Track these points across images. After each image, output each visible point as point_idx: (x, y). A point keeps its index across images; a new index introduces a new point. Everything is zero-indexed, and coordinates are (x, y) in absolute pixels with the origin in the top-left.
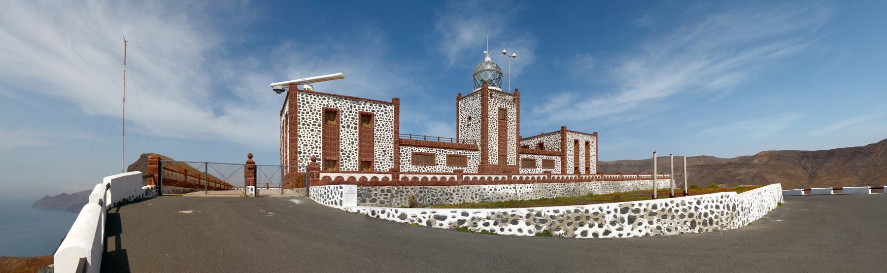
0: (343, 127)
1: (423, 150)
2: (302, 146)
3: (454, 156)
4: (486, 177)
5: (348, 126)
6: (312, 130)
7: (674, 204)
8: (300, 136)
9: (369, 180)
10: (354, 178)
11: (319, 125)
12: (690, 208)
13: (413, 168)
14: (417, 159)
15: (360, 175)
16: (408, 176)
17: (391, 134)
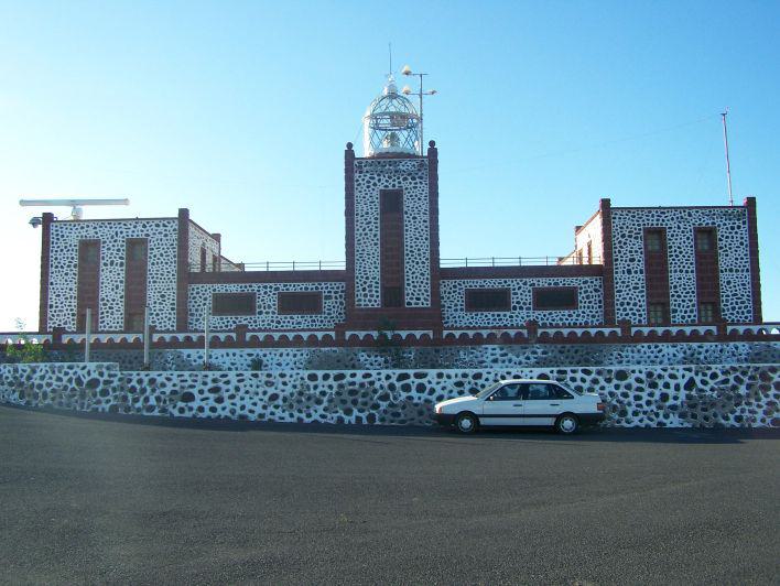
0: (105, 265)
1: (234, 288)
3: (294, 295)
4: (389, 334)
5: (112, 263)
6: (66, 274)
8: (52, 284)
9: (167, 340)
11: (75, 266)
12: (22, 376)
13: (216, 320)
14: (223, 305)
15: (663, 329)
16: (302, 334)
17: (173, 268)
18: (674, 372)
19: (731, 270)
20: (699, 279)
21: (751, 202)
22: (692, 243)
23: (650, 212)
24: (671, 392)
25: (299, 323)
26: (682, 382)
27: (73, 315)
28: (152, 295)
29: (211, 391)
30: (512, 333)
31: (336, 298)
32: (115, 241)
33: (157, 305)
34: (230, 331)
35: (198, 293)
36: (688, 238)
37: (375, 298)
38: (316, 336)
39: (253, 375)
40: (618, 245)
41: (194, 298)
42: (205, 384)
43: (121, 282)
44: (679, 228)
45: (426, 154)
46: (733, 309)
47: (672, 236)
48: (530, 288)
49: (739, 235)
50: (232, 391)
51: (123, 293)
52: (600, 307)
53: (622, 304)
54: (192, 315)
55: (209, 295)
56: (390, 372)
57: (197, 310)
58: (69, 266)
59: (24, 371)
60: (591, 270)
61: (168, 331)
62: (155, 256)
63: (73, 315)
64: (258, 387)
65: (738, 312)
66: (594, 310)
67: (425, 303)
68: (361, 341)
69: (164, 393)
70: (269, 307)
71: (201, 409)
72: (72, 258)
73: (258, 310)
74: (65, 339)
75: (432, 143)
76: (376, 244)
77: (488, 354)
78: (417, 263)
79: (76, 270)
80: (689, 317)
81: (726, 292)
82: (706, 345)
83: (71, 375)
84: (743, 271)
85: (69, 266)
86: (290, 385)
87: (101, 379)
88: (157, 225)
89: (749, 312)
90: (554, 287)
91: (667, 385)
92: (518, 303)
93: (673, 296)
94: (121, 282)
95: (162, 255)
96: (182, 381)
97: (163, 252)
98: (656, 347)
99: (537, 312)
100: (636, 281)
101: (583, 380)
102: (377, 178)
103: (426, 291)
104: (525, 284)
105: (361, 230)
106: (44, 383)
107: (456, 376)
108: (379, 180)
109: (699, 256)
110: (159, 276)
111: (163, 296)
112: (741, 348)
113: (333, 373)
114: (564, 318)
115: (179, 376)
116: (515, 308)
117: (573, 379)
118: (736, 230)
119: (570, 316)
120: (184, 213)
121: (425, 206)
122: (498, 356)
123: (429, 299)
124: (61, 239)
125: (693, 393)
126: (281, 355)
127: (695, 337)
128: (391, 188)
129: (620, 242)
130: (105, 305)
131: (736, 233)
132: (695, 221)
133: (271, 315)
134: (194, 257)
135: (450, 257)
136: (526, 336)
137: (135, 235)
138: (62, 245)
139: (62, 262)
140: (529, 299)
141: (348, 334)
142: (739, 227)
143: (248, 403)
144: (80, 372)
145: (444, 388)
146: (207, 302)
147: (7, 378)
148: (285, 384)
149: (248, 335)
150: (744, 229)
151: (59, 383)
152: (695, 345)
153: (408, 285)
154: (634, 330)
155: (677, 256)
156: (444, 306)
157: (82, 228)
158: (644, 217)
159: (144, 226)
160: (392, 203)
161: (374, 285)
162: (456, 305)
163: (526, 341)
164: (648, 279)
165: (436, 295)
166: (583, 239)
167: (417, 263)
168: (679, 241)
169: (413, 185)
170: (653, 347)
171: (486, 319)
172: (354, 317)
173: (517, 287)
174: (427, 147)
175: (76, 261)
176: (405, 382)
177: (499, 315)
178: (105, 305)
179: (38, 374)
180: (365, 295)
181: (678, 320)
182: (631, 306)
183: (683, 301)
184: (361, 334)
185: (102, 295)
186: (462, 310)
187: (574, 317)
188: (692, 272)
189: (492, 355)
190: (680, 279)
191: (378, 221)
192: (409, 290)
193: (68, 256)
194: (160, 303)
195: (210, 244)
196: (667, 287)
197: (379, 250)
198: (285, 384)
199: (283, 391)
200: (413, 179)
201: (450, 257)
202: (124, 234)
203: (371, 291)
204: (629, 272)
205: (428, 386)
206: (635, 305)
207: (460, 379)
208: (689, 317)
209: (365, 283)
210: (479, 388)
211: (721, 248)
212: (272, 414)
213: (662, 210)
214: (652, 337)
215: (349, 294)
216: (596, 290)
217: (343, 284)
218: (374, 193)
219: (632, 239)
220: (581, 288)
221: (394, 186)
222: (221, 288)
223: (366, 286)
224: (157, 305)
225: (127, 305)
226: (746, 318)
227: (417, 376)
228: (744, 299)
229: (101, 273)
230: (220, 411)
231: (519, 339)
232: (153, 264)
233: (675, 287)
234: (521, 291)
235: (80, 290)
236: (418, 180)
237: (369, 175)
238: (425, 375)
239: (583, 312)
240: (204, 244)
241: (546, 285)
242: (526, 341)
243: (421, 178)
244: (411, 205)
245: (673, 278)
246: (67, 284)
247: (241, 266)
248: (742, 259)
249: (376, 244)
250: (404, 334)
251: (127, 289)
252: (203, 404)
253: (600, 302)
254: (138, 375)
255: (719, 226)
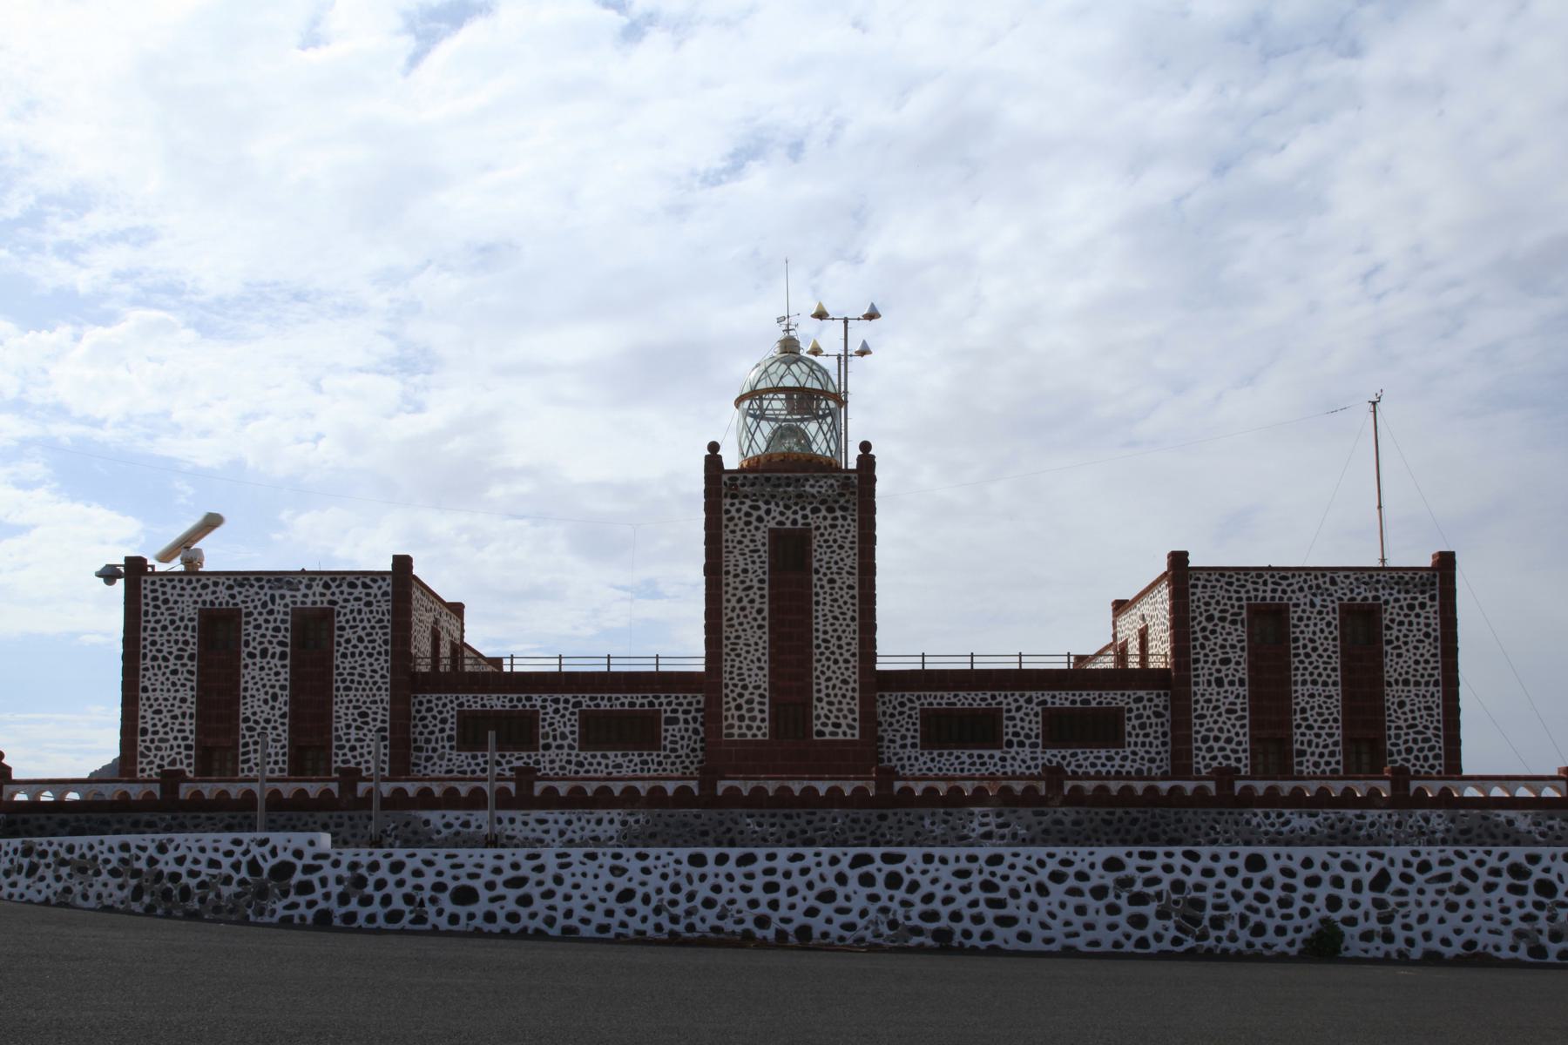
0: (251, 655)
1: (497, 702)
2: (149, 714)
5: (264, 653)
6: (174, 672)
7: (104, 848)
8: (145, 690)
10: (635, 790)
11: (191, 657)
17: (383, 663)
18: (1352, 858)
19: (1406, 682)
20: (1348, 697)
21: (1446, 562)
22: (1336, 633)
23: (1260, 576)
24: (1346, 894)
25: (619, 767)
26: (1367, 877)
27: (188, 747)
28: (343, 712)
29: (507, 884)
30: (1018, 787)
31: (686, 721)
32: (271, 612)
33: (352, 731)
34: (1031, 777)
35: (429, 710)
36: (1329, 624)
37: (758, 723)
38: (663, 790)
39: (587, 856)
40: (1199, 635)
41: (423, 718)
42: (497, 871)
43: (283, 688)
44: (1313, 605)
45: (853, 465)
46: (1409, 751)
47: (1300, 619)
48: (1039, 709)
49: (1422, 620)
50: (550, 885)
51: (286, 709)
52: (1164, 744)
53: (1205, 740)
54: (420, 749)
55: (450, 713)
56: (837, 851)
57: (428, 741)
58: (179, 658)
59: (144, 849)
60: (1147, 678)
61: (1139, 775)
62: (348, 641)
63: (188, 747)
64: (596, 876)
65: (1417, 758)
66: (1153, 750)
67: (849, 731)
68: (465, 799)
69: (419, 888)
70: (564, 737)
71: (490, 917)
72: (186, 643)
73: (542, 742)
74: (185, 791)
75: (866, 446)
76: (760, 627)
77: (975, 824)
78: (836, 662)
79: (193, 666)
80: (1328, 763)
81: (1396, 720)
82: (1372, 814)
83: (238, 855)
84: (1427, 684)
85: (179, 658)
86: (656, 874)
87: (299, 864)
88: (352, 585)
89: (1436, 757)
90: (1079, 702)
91: (1338, 882)
92: (1016, 734)
93: (1299, 726)
94: (283, 688)
95: (360, 639)
96: (454, 866)
97: (363, 634)
98: (1280, 815)
99: (1049, 752)
100: (1232, 698)
101: (1186, 870)
102: (764, 507)
103: (852, 711)
104: (1029, 701)
105: (734, 600)
106: (182, 870)
107: (957, 859)
108: (768, 512)
109: (1348, 657)
110: (356, 678)
111: (363, 715)
112: (1434, 821)
113: (735, 853)
114: (1099, 762)
115: (448, 857)
116: (1010, 744)
117: (1168, 869)
118: (1417, 610)
119: (1109, 758)
120: (403, 563)
121: (851, 560)
122: (993, 827)
123: (857, 724)
124: (163, 608)
125: (1386, 896)
126: (599, 822)
127: (1348, 799)
128: (788, 525)
129: (1204, 629)
130: (250, 729)
131: (1418, 616)
132: (1342, 592)
133: (566, 751)
134: (421, 644)
135: (896, 648)
136: (1043, 793)
137: (309, 601)
138: (166, 619)
139: (165, 649)
140: (1037, 728)
141: (722, 786)
142: (1423, 606)
143: (577, 905)
144: (256, 851)
145: (934, 881)
146: (447, 726)
147: (107, 861)
148: (646, 871)
149: (539, 787)
150: (1433, 609)
151: (214, 871)
152: (1350, 813)
153: (819, 700)
154: (1239, 785)
155: (1308, 655)
156: (882, 739)
157: (205, 587)
158: (1250, 586)
159: (327, 586)
160: (791, 556)
161: (757, 699)
162: (904, 737)
163: (1043, 801)
164: (1254, 696)
165: (869, 719)
166: (1129, 627)
167: (836, 662)
168: (1312, 628)
169: (829, 522)
170: (1273, 815)
171: (961, 765)
172: (719, 756)
173: (1013, 706)
174: (854, 453)
175: (192, 649)
176: (865, 869)
177: (980, 757)
178: (250, 729)
179: (171, 855)
180: (741, 718)
181: (1308, 768)
182: (1221, 743)
183: (1318, 736)
184: (746, 787)
185: (245, 711)
186: (914, 745)
187: (1117, 762)
188: (1335, 684)
189: (982, 825)
190: (1312, 696)
191: (766, 586)
192: (821, 709)
193: (176, 638)
194: (358, 728)
195: (447, 622)
196: (1289, 712)
197: (766, 637)
198: (646, 871)
199: (643, 884)
200: (831, 510)
201: (896, 648)
202: (288, 600)
203: (750, 710)
204: (1219, 682)
205: (907, 878)
206: (1229, 740)
207: (964, 865)
208: (1328, 763)
209: (741, 695)
210: (997, 880)
211: (1389, 642)
212: (623, 925)
213: (1282, 574)
214: (1272, 799)
215: (712, 716)
216: (1158, 715)
217: (700, 697)
218: (759, 535)
219: (1227, 625)
220: (1130, 710)
221: (795, 522)
222: (474, 702)
223: (741, 701)
224: (352, 731)
225: (294, 730)
226: (1432, 767)
227: (888, 859)
228: (1429, 733)
229: (243, 671)
230: (525, 921)
231: (1029, 798)
232: (344, 656)
233: (1303, 711)
234: (1021, 714)
235: (201, 701)
236: (839, 513)
237: (749, 503)
238: (900, 858)
239: (1134, 753)
240: (436, 622)
241: (1067, 704)
242: (1043, 801)
243: (843, 509)
244: (826, 558)
245: (1300, 693)
246: (175, 692)
247: (497, 662)
248: (1427, 662)
249: (760, 627)
250: (822, 787)
251: (294, 701)
252: (495, 907)
253: (1164, 734)
254: (371, 854)
255: (1387, 602)
